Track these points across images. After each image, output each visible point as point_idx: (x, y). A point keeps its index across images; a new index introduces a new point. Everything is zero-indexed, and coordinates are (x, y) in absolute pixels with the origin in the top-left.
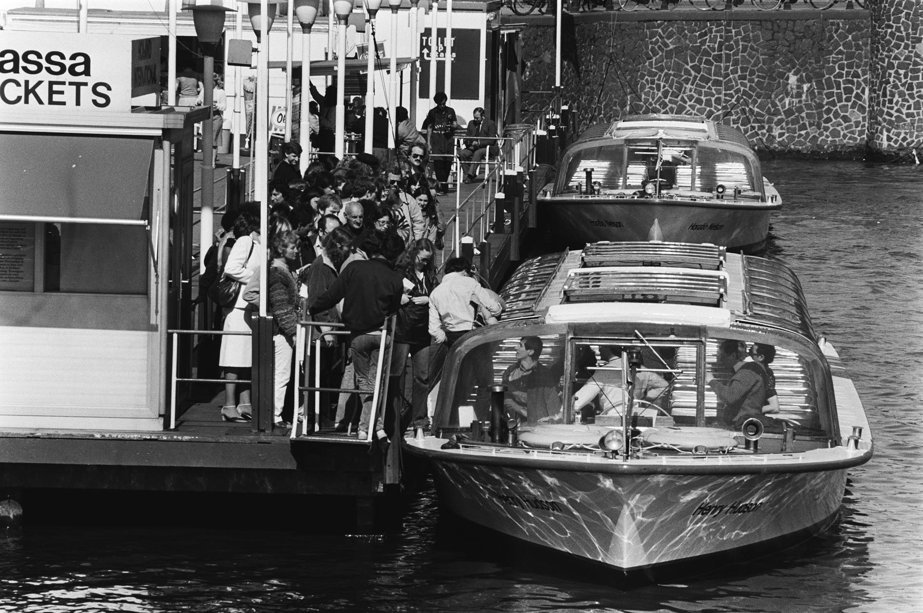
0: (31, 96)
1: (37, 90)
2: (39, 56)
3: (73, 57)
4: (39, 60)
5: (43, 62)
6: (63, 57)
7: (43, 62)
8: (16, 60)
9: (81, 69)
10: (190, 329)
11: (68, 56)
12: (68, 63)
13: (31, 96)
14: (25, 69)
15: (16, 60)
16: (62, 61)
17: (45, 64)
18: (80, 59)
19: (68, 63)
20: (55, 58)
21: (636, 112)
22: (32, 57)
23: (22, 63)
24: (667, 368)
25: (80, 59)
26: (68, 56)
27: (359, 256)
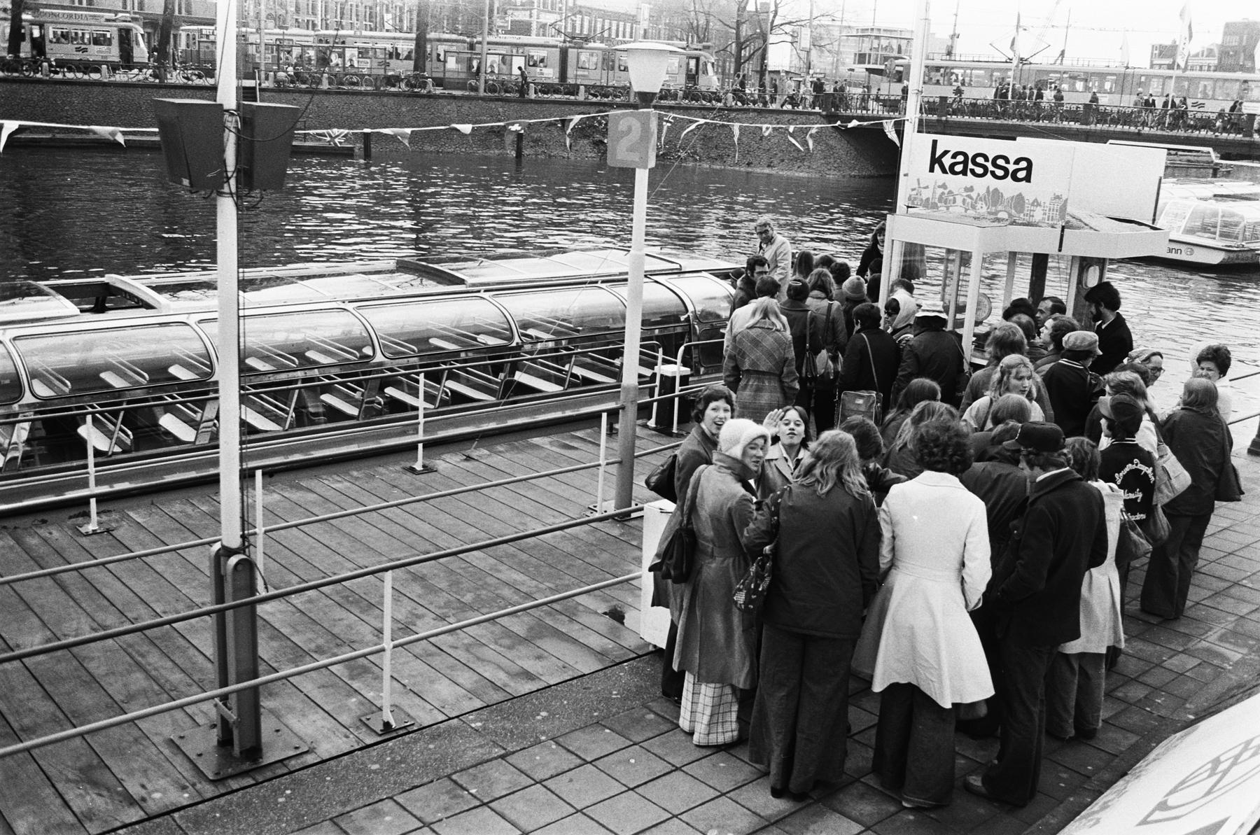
0: (937, 166)
1: (943, 160)
2: (986, 159)
3: (1017, 162)
4: (986, 163)
5: (989, 165)
6: (1007, 161)
7: (989, 165)
8: (965, 163)
9: (1021, 174)
10: (679, 423)
11: (1012, 161)
12: (1011, 167)
13: (937, 166)
14: (973, 171)
15: (965, 163)
16: (1007, 166)
17: (991, 168)
18: (1023, 164)
19: (1011, 167)
20: (1001, 162)
21: (199, 501)
22: (980, 160)
23: (971, 166)
24: (571, 120)
25: (1023, 164)
26: (1012, 161)
27: (798, 387)
